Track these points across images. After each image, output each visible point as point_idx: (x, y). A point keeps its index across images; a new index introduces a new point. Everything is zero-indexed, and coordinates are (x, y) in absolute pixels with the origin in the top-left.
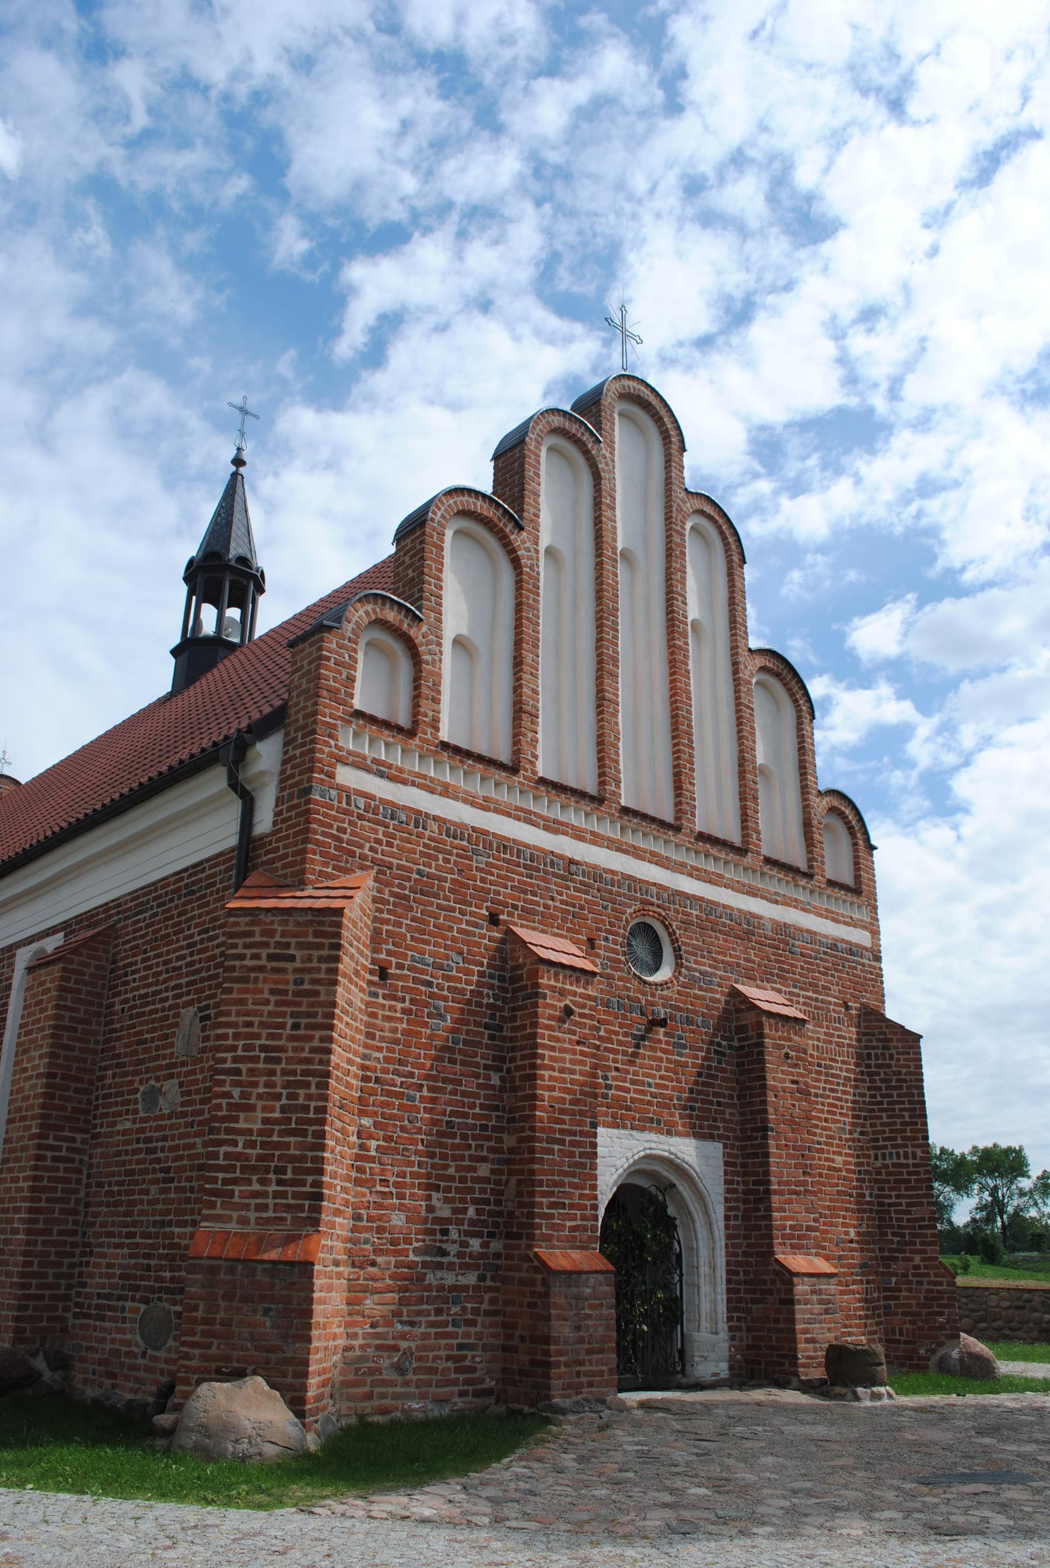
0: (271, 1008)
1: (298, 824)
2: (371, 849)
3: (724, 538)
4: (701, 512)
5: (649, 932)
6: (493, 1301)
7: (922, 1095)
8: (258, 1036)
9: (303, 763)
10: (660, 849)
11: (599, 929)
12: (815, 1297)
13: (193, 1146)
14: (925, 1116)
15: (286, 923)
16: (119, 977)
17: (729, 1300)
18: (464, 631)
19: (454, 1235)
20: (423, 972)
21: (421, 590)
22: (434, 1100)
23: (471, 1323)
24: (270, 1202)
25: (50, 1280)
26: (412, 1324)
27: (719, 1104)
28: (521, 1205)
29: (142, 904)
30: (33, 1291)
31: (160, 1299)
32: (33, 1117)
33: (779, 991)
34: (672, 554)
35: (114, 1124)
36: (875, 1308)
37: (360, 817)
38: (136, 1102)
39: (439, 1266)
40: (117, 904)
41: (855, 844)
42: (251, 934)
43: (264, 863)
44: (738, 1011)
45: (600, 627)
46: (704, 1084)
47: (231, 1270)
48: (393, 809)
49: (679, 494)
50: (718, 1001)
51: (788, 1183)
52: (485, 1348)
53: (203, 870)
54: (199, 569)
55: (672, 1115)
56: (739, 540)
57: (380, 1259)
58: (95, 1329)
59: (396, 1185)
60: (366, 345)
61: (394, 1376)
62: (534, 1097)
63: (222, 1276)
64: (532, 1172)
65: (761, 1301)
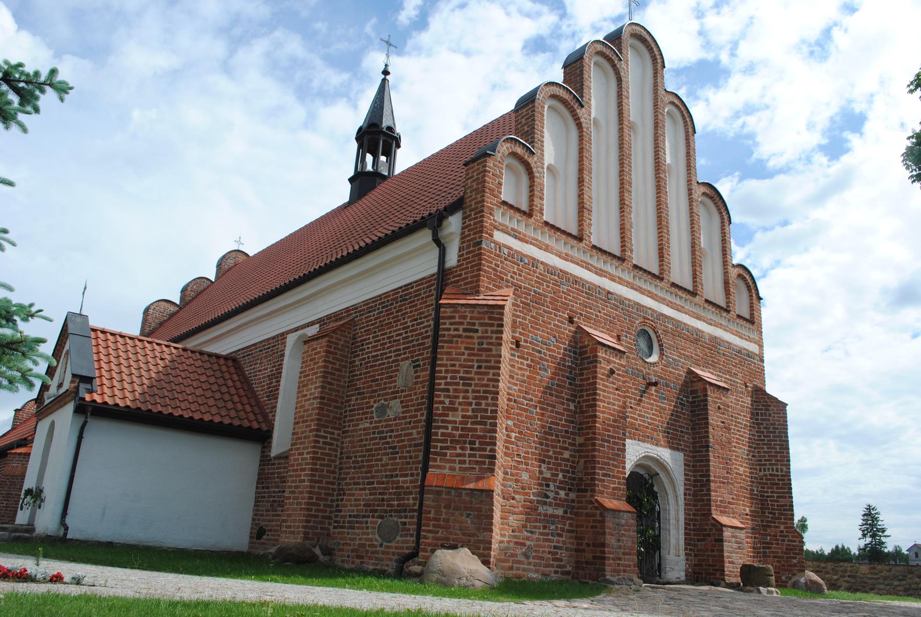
0: (465, 357)
1: (474, 261)
2: (511, 277)
3: (684, 118)
4: (672, 103)
5: (650, 333)
6: (571, 525)
7: (787, 437)
8: (458, 372)
9: (476, 228)
10: (653, 290)
11: (622, 330)
12: (733, 539)
13: (411, 434)
14: (788, 449)
15: (473, 312)
16: (358, 347)
17: (686, 539)
18: (552, 162)
19: (552, 488)
20: (537, 345)
21: (533, 137)
22: (542, 415)
23: (560, 535)
24: (467, 459)
25: (322, 507)
26: (532, 532)
27: (682, 432)
28: (587, 474)
29: (372, 307)
30: (313, 513)
31: (391, 516)
32: (311, 420)
33: (712, 373)
34: (657, 125)
35: (358, 425)
36: (758, 553)
37: (506, 259)
38: (372, 412)
39: (545, 503)
40: (355, 307)
41: (751, 296)
42: (454, 317)
43: (452, 283)
44: (692, 382)
45: (621, 164)
46: (674, 420)
47: (449, 493)
48: (522, 256)
49: (661, 92)
50: (681, 376)
51: (719, 477)
52: (567, 549)
53: (412, 287)
54: (365, 132)
55: (658, 435)
56: (692, 120)
57: (517, 497)
58: (348, 533)
59: (525, 458)
60: (417, 16)
61: (523, 559)
62: (595, 416)
63: (444, 496)
64: (594, 456)
65: (703, 540)
